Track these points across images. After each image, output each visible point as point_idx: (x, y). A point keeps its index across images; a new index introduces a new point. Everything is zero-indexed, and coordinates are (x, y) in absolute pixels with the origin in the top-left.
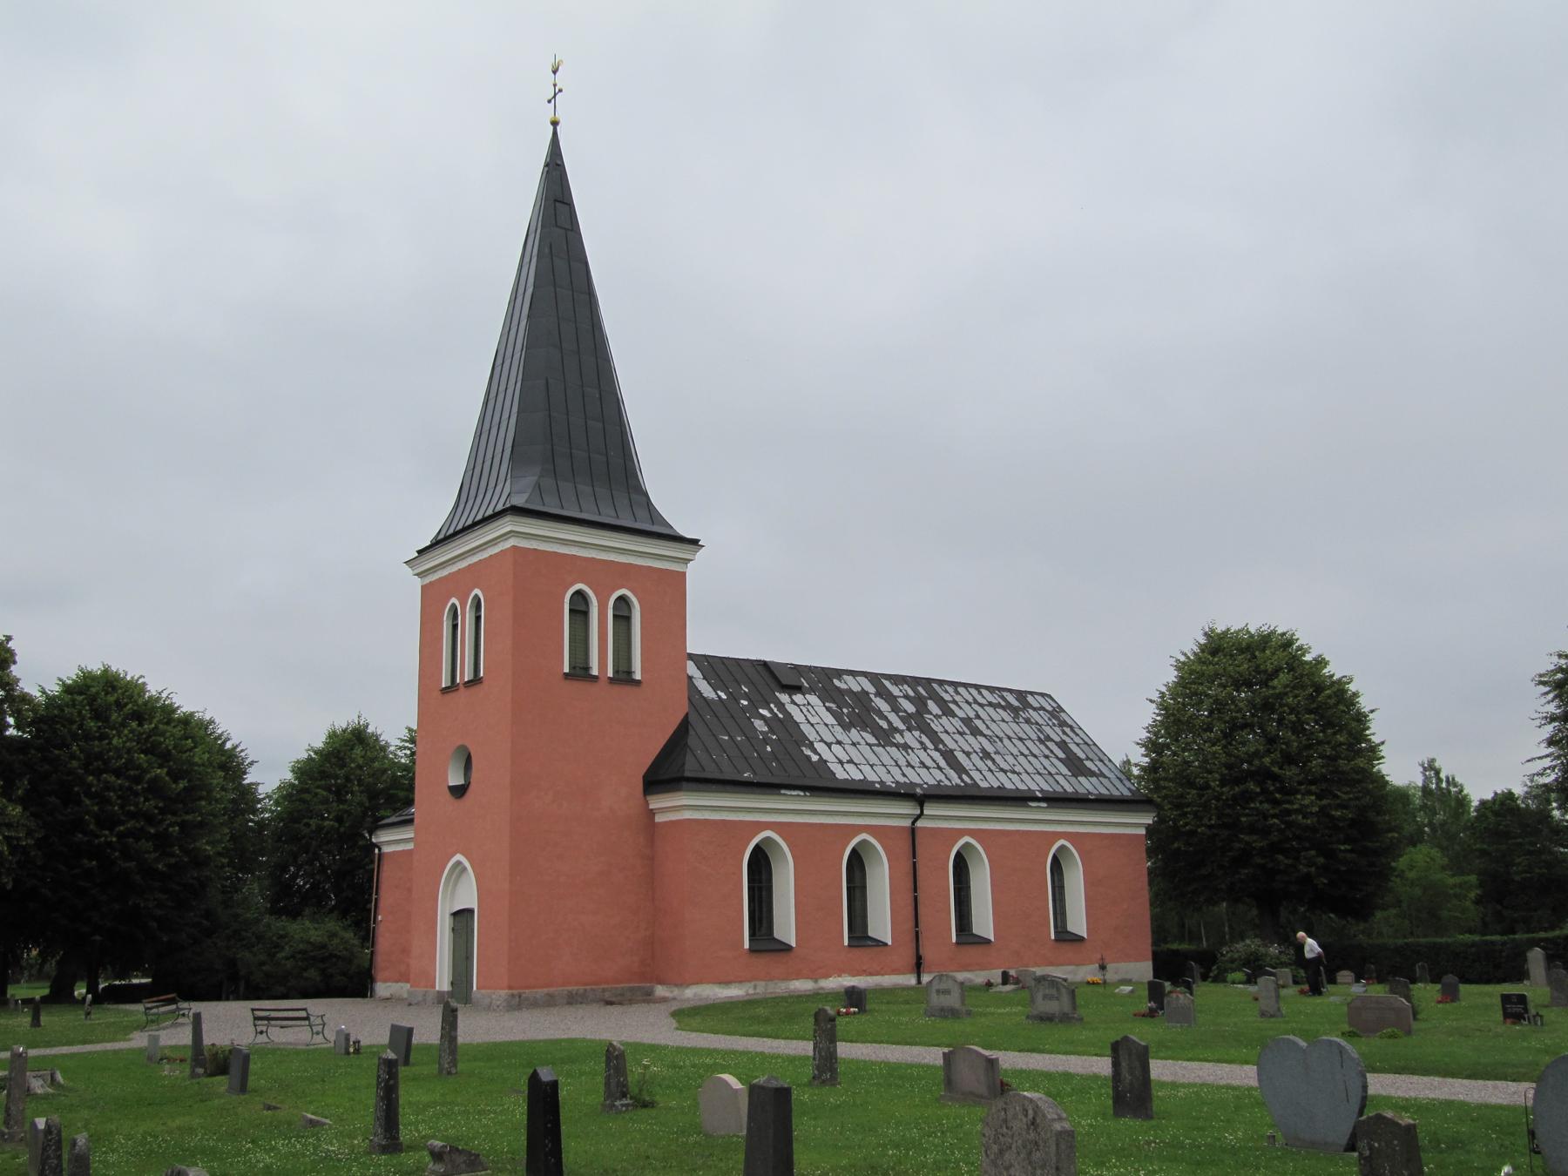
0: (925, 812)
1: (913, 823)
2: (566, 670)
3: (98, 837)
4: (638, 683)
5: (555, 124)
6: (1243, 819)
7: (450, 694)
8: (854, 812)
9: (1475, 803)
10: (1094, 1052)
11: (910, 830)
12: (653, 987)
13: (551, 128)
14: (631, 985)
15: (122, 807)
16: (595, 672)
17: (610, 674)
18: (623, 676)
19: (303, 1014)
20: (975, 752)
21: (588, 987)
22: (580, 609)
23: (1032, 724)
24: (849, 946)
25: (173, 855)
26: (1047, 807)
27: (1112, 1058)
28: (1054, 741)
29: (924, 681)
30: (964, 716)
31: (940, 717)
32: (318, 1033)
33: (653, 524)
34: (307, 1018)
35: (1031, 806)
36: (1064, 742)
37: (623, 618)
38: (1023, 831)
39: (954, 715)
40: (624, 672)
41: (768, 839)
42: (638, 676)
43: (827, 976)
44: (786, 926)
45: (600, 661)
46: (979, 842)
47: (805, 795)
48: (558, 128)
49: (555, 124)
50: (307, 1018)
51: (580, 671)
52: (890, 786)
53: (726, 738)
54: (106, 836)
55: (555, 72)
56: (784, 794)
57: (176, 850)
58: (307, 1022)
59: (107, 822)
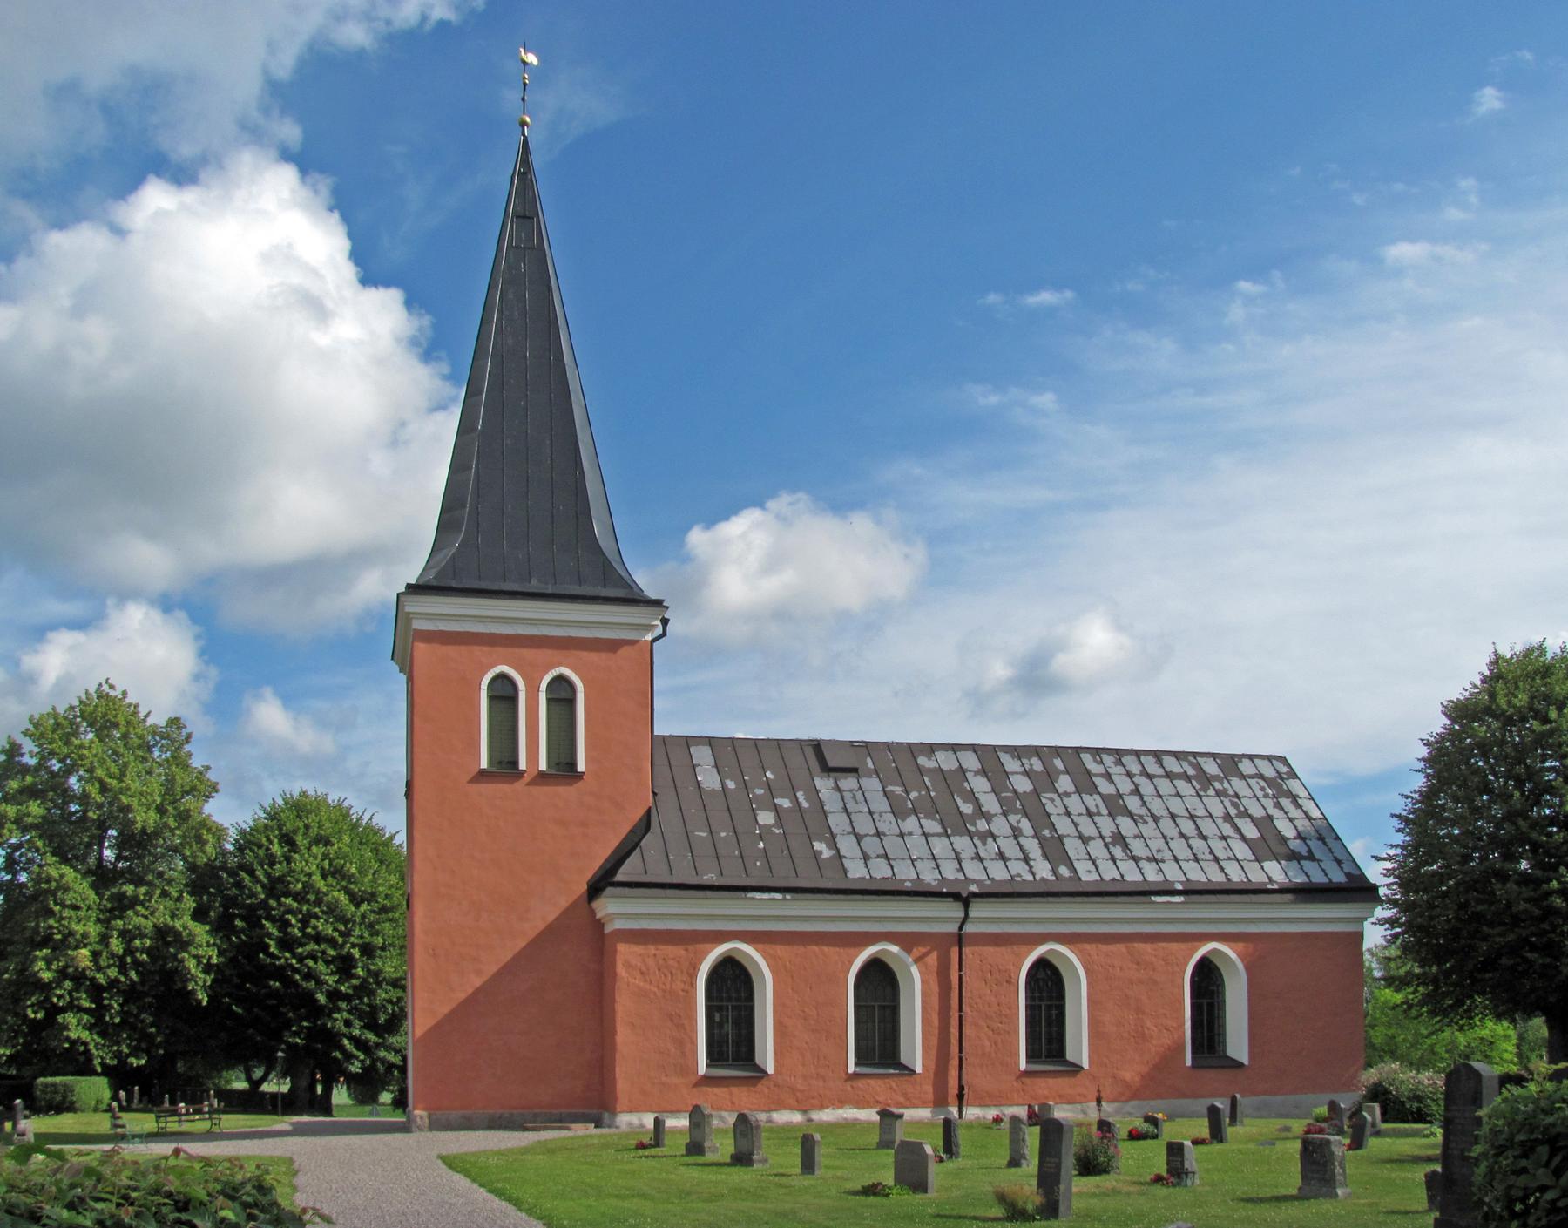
0: (972, 914)
1: (961, 928)
2: (484, 764)
3: (279, 959)
8: (778, 916)
9: (233, 834)
11: (957, 938)
12: (601, 1113)
14: (574, 1111)
15: (302, 930)
16: (522, 765)
18: (564, 768)
20: (1102, 837)
21: (515, 1112)
22: (504, 694)
23: (1227, 796)
24: (1193, 1066)
25: (357, 977)
26: (791, 899)
28: (1250, 817)
29: (1070, 751)
30: (1112, 790)
31: (1068, 795)
33: (505, 581)
35: (1154, 903)
36: (1270, 818)
37: (562, 695)
39: (1094, 790)
41: (1215, 951)
42: (581, 767)
43: (822, 1107)
44: (1237, 1044)
45: (535, 753)
47: (784, 899)
51: (505, 765)
52: (930, 884)
53: (704, 834)
54: (287, 959)
56: (753, 899)
57: (360, 972)
59: (287, 943)
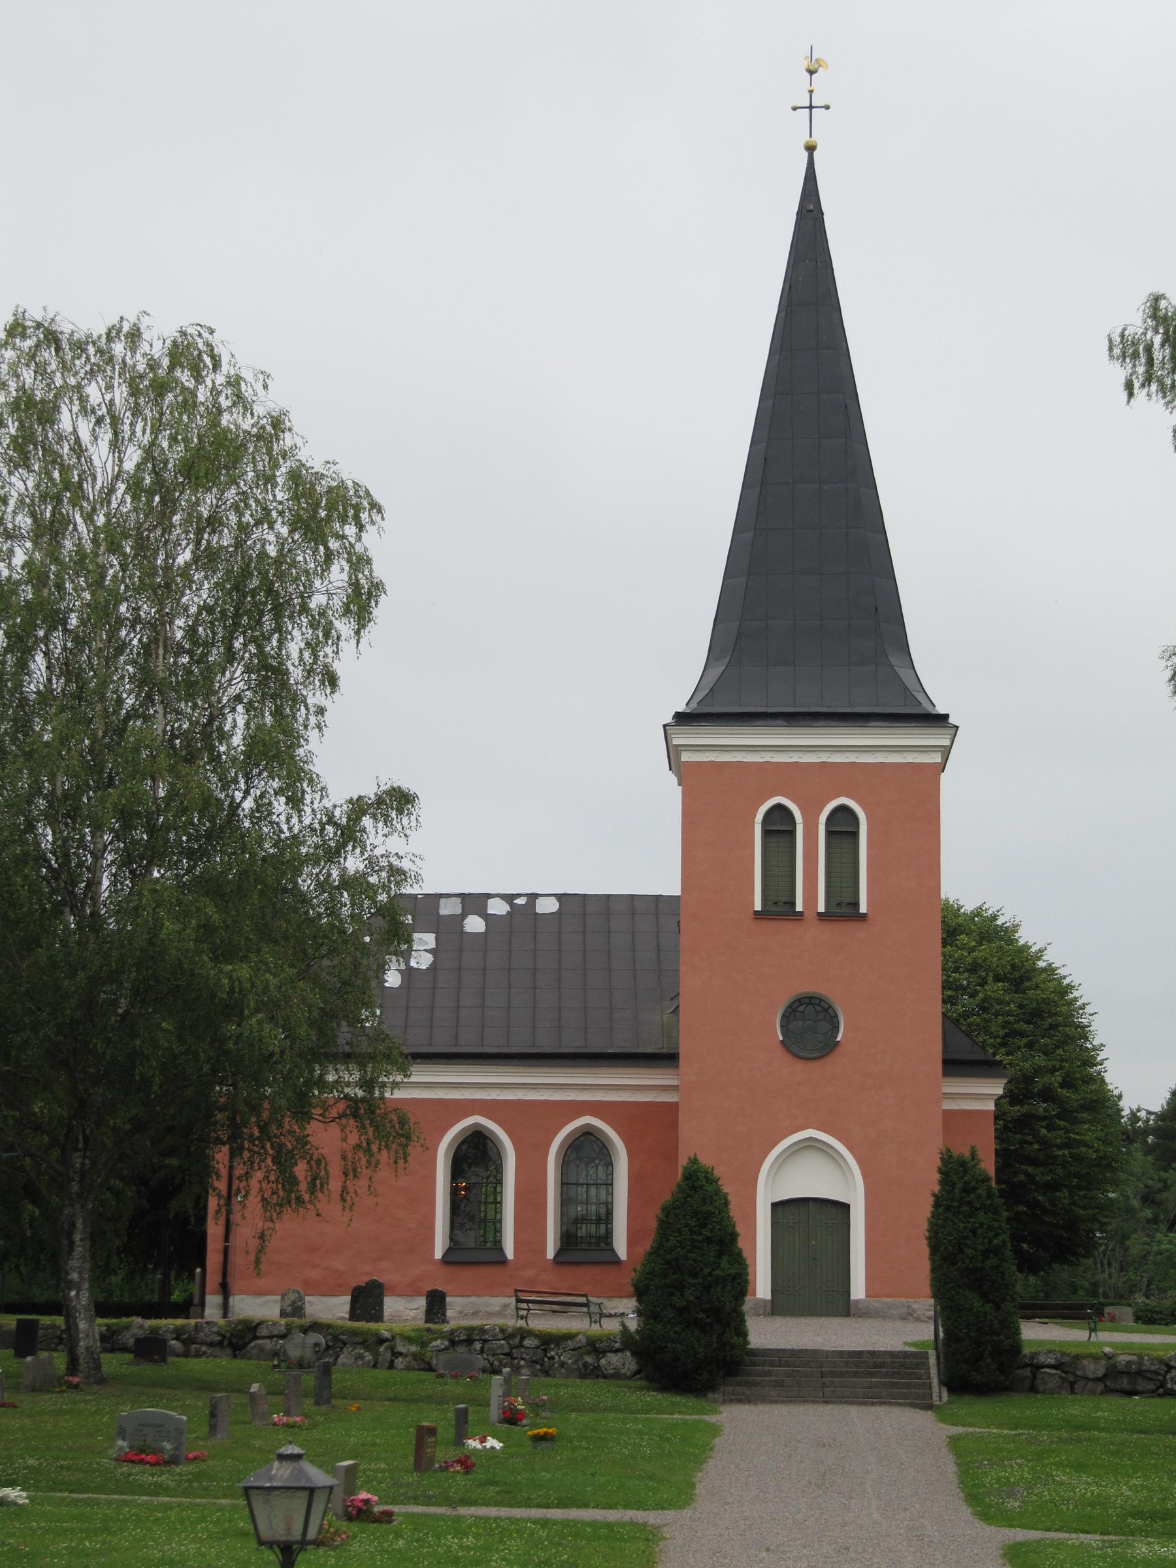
4: (864, 917)
5: (811, 149)
6: (73, 1293)
7: (786, 922)
10: (417, 1367)
13: (806, 154)
17: (821, 908)
19: (583, 1300)
27: (1020, 1340)
32: (595, 1322)
34: (586, 1305)
38: (972, 1111)
40: (849, 904)
42: (863, 909)
46: (839, 1138)
48: (816, 154)
49: (811, 149)
50: (586, 1305)
55: (811, 72)
58: (585, 1309)
